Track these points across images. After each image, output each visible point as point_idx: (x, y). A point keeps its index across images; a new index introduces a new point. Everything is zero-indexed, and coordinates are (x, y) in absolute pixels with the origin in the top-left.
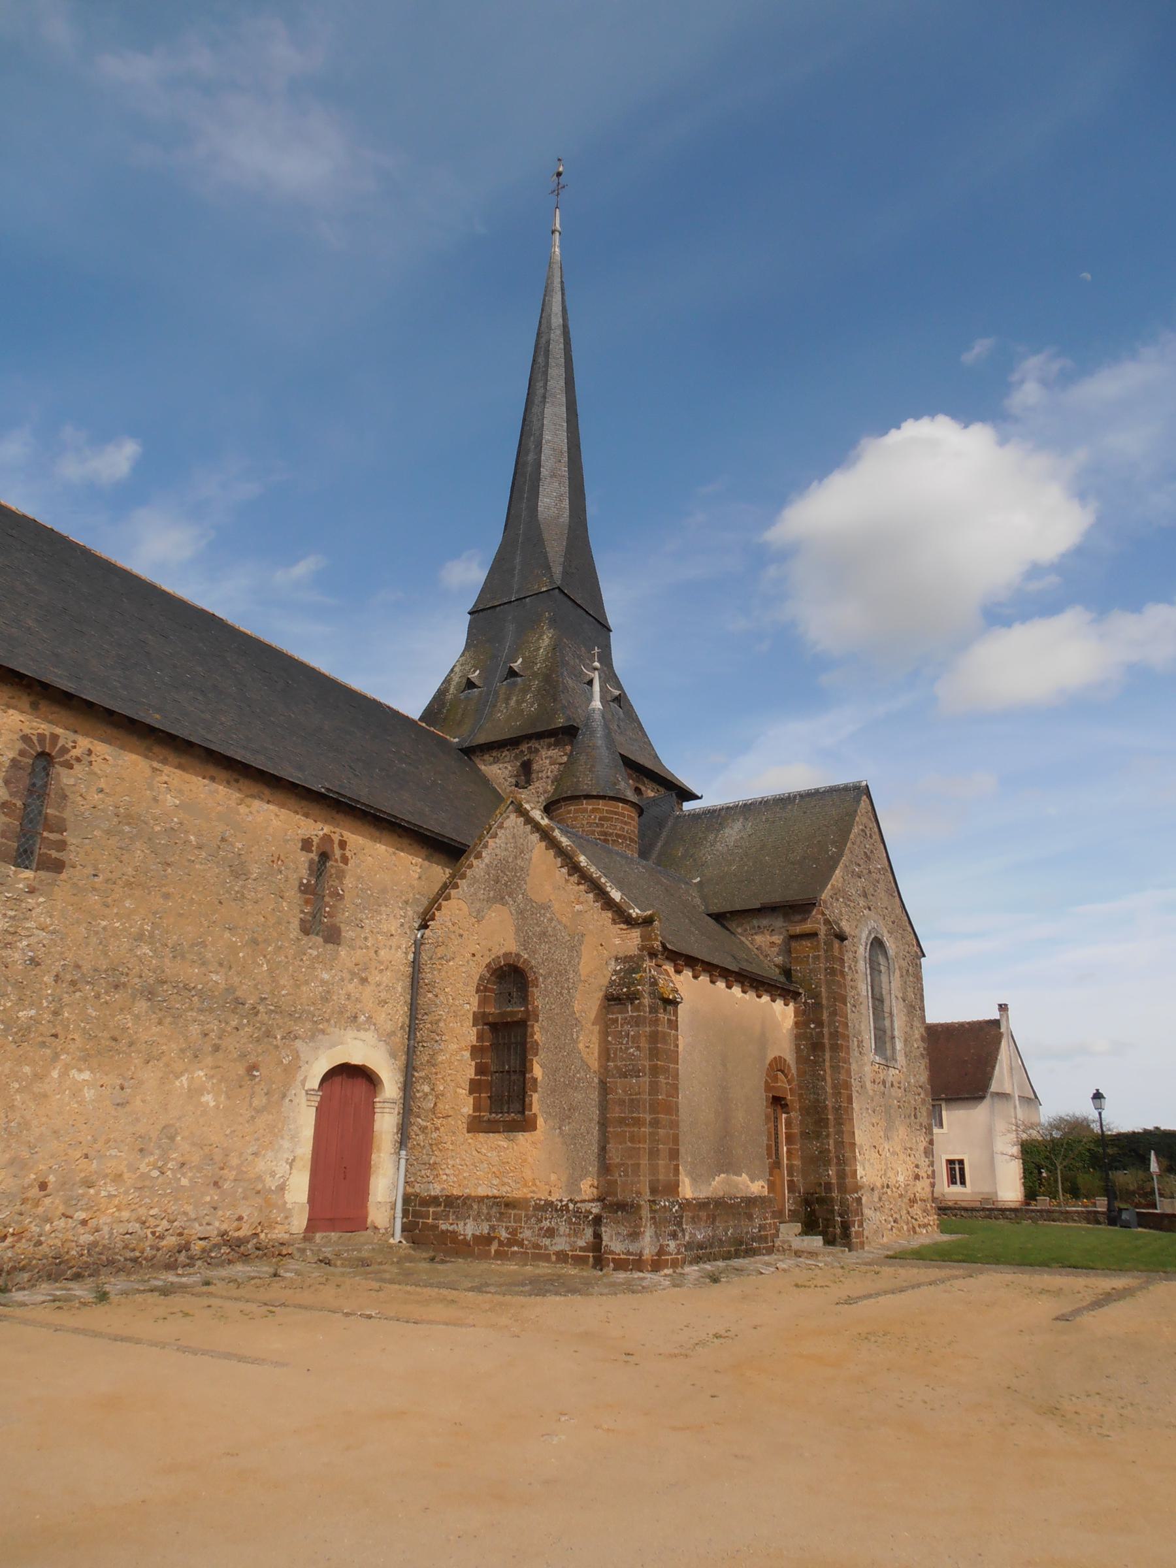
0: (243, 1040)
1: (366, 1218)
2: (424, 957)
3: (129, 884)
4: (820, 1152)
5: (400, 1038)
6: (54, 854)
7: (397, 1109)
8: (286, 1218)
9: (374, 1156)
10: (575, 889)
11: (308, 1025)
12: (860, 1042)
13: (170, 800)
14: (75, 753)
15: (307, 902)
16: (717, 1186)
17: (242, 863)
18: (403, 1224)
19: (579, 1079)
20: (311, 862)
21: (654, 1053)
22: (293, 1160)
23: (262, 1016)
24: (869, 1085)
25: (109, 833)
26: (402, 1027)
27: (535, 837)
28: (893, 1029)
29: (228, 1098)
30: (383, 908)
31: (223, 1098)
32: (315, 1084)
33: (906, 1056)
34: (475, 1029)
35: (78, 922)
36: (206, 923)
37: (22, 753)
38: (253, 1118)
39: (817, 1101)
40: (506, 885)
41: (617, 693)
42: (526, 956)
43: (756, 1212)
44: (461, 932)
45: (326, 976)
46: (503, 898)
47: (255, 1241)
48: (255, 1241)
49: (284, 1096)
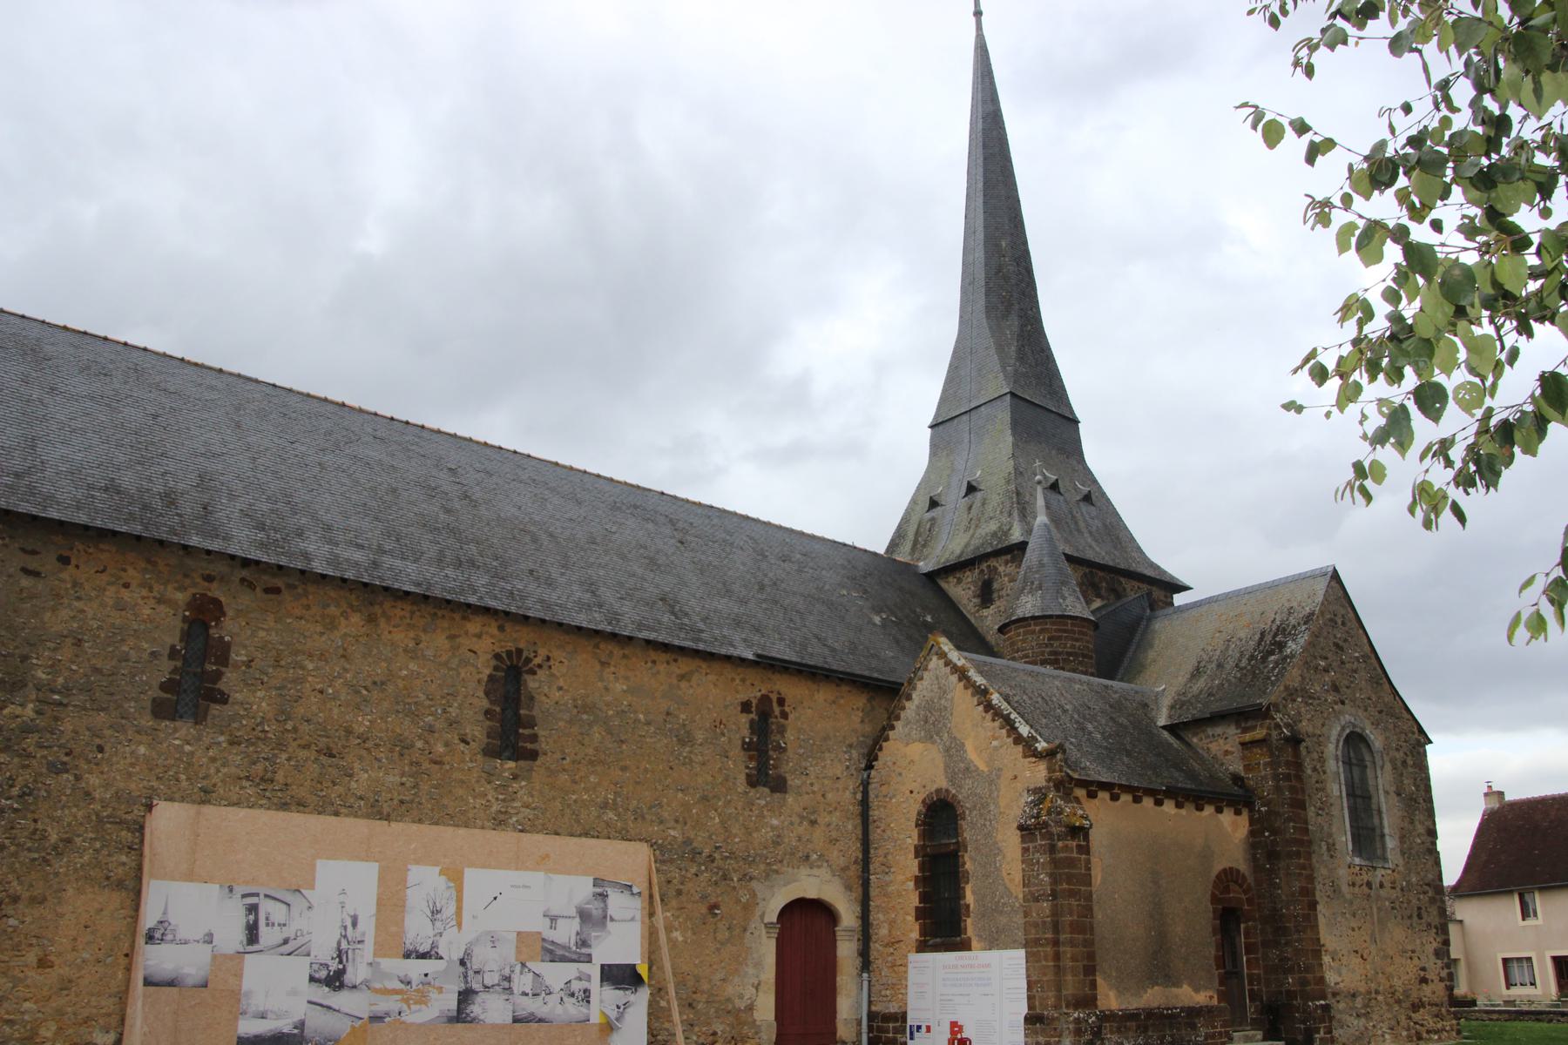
2: (872, 795)
3: (591, 763)
5: (855, 870)
6: (529, 746)
10: (992, 726)
11: (762, 867)
12: (1331, 847)
13: (619, 687)
14: (537, 661)
15: (751, 758)
16: (1153, 997)
20: (752, 721)
23: (719, 862)
24: (1345, 889)
25: (571, 722)
28: (1382, 827)
32: (772, 917)
33: (1403, 853)
35: (554, 798)
37: (496, 668)
38: (718, 950)
40: (934, 725)
41: (1085, 490)
43: (1200, 1022)
45: (775, 822)
49: (745, 930)
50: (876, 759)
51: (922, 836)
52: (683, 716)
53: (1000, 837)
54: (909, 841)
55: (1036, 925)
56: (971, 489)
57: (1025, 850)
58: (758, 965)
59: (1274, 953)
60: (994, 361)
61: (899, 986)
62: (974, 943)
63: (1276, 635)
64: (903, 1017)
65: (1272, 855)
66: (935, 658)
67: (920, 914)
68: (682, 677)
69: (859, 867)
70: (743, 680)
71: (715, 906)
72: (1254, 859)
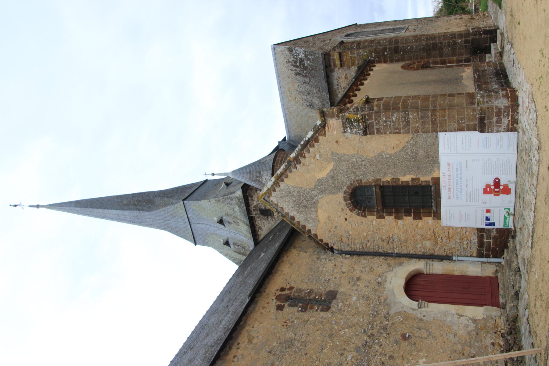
0: (388, 342)
1: (490, 277)
2: (348, 249)
4: (449, 46)
5: (390, 260)
7: (430, 262)
8: (492, 318)
9: (456, 274)
11: (381, 307)
17: (285, 342)
18: (494, 257)
19: (411, 152)
20: (290, 305)
21: (396, 109)
22: (458, 315)
23: (375, 332)
26: (386, 260)
27: (282, 184)
29: (421, 350)
30: (320, 269)
31: (421, 354)
32: (415, 304)
34: (386, 217)
36: (317, 363)
39: (423, 49)
40: (307, 202)
42: (345, 188)
44: (334, 227)
45: (354, 298)
46: (315, 203)
47: (506, 335)
48: (506, 335)
49: (421, 320)
50: (327, 244)
51: (371, 213)
52: (275, 343)
53: (371, 155)
54: (374, 222)
55: (423, 123)
56: (221, 222)
57: (378, 131)
58: (445, 314)
59: (446, 50)
60: (170, 208)
61: (460, 232)
62: (435, 175)
63: (297, 67)
64: (480, 230)
65: (396, 50)
66: (271, 198)
67: (417, 217)
68: (250, 341)
69: (389, 258)
70: (264, 308)
71: (404, 337)
72: (397, 61)
